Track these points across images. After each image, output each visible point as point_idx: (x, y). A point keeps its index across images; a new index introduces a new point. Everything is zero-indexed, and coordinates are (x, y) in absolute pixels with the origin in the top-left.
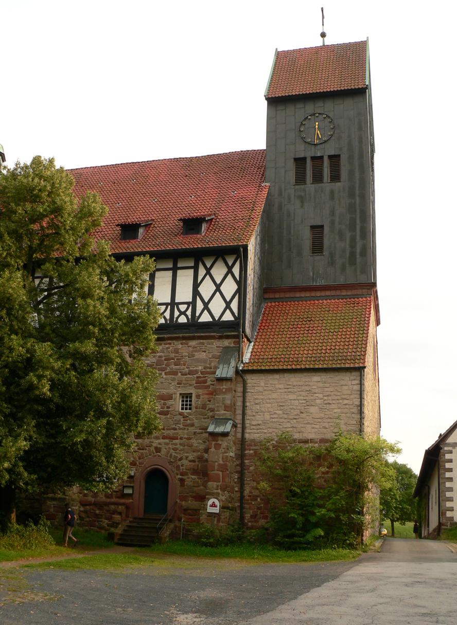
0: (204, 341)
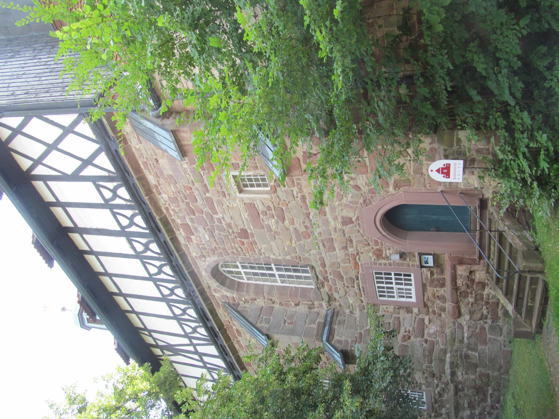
0: (140, 162)
